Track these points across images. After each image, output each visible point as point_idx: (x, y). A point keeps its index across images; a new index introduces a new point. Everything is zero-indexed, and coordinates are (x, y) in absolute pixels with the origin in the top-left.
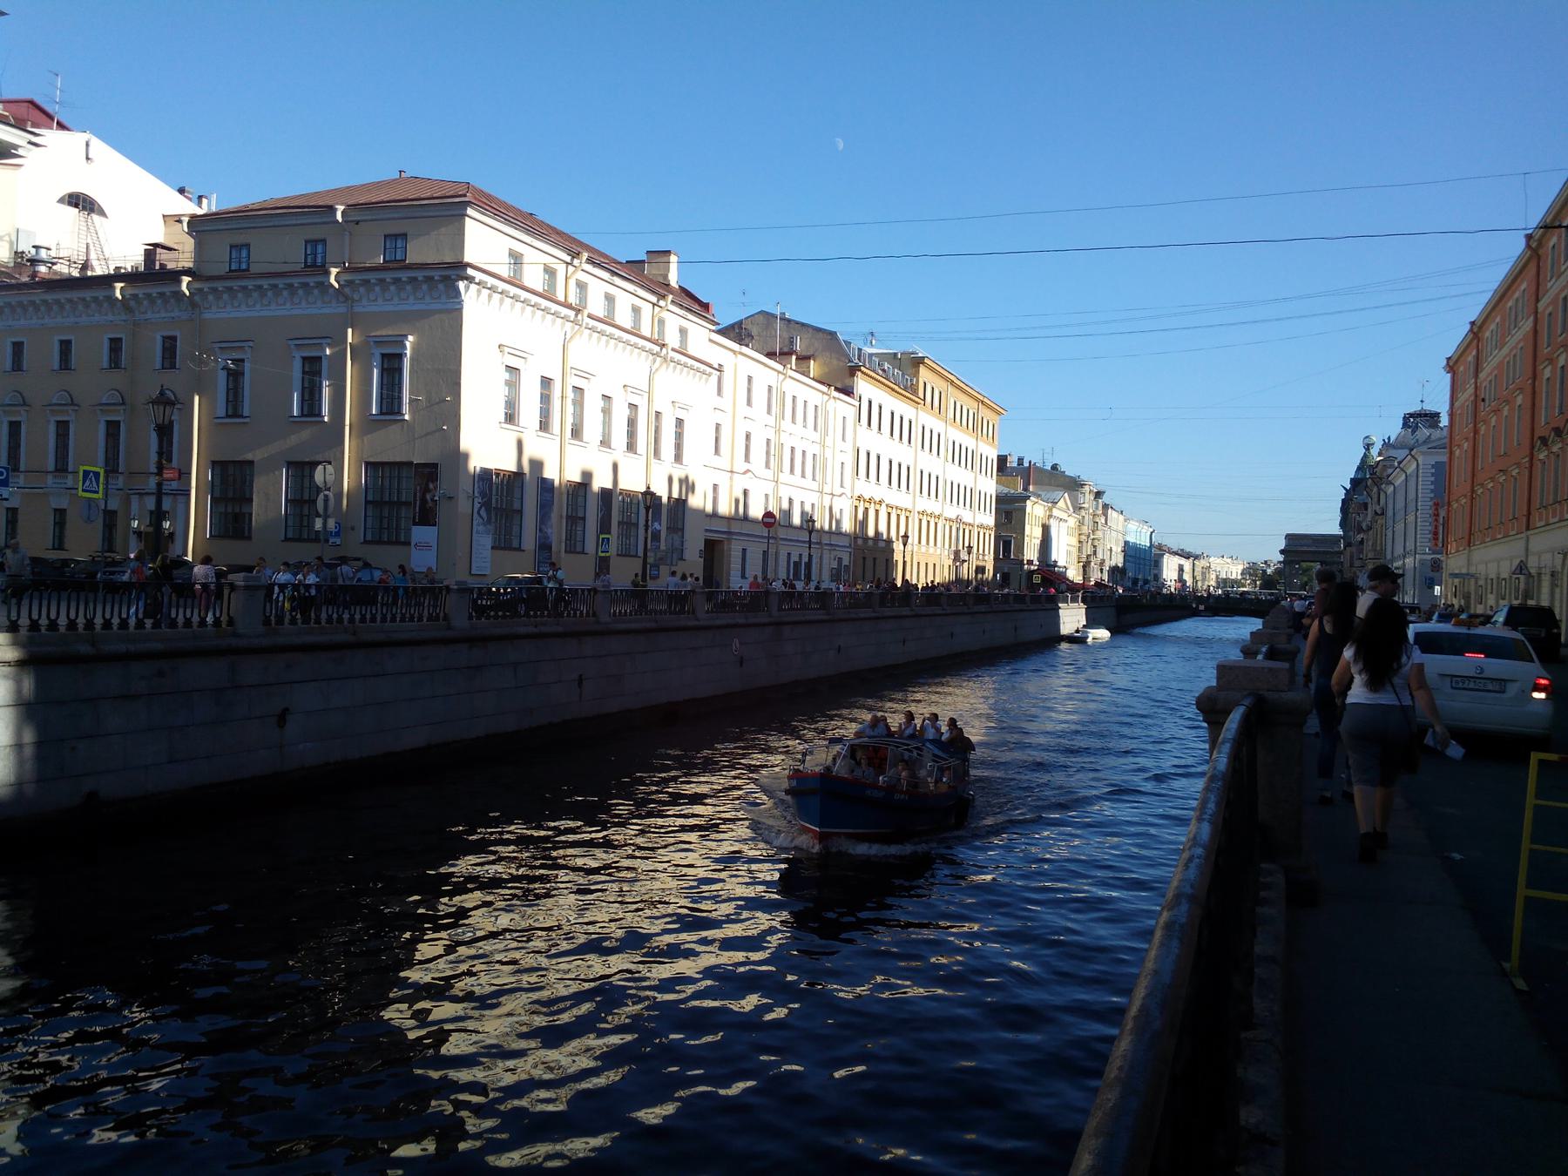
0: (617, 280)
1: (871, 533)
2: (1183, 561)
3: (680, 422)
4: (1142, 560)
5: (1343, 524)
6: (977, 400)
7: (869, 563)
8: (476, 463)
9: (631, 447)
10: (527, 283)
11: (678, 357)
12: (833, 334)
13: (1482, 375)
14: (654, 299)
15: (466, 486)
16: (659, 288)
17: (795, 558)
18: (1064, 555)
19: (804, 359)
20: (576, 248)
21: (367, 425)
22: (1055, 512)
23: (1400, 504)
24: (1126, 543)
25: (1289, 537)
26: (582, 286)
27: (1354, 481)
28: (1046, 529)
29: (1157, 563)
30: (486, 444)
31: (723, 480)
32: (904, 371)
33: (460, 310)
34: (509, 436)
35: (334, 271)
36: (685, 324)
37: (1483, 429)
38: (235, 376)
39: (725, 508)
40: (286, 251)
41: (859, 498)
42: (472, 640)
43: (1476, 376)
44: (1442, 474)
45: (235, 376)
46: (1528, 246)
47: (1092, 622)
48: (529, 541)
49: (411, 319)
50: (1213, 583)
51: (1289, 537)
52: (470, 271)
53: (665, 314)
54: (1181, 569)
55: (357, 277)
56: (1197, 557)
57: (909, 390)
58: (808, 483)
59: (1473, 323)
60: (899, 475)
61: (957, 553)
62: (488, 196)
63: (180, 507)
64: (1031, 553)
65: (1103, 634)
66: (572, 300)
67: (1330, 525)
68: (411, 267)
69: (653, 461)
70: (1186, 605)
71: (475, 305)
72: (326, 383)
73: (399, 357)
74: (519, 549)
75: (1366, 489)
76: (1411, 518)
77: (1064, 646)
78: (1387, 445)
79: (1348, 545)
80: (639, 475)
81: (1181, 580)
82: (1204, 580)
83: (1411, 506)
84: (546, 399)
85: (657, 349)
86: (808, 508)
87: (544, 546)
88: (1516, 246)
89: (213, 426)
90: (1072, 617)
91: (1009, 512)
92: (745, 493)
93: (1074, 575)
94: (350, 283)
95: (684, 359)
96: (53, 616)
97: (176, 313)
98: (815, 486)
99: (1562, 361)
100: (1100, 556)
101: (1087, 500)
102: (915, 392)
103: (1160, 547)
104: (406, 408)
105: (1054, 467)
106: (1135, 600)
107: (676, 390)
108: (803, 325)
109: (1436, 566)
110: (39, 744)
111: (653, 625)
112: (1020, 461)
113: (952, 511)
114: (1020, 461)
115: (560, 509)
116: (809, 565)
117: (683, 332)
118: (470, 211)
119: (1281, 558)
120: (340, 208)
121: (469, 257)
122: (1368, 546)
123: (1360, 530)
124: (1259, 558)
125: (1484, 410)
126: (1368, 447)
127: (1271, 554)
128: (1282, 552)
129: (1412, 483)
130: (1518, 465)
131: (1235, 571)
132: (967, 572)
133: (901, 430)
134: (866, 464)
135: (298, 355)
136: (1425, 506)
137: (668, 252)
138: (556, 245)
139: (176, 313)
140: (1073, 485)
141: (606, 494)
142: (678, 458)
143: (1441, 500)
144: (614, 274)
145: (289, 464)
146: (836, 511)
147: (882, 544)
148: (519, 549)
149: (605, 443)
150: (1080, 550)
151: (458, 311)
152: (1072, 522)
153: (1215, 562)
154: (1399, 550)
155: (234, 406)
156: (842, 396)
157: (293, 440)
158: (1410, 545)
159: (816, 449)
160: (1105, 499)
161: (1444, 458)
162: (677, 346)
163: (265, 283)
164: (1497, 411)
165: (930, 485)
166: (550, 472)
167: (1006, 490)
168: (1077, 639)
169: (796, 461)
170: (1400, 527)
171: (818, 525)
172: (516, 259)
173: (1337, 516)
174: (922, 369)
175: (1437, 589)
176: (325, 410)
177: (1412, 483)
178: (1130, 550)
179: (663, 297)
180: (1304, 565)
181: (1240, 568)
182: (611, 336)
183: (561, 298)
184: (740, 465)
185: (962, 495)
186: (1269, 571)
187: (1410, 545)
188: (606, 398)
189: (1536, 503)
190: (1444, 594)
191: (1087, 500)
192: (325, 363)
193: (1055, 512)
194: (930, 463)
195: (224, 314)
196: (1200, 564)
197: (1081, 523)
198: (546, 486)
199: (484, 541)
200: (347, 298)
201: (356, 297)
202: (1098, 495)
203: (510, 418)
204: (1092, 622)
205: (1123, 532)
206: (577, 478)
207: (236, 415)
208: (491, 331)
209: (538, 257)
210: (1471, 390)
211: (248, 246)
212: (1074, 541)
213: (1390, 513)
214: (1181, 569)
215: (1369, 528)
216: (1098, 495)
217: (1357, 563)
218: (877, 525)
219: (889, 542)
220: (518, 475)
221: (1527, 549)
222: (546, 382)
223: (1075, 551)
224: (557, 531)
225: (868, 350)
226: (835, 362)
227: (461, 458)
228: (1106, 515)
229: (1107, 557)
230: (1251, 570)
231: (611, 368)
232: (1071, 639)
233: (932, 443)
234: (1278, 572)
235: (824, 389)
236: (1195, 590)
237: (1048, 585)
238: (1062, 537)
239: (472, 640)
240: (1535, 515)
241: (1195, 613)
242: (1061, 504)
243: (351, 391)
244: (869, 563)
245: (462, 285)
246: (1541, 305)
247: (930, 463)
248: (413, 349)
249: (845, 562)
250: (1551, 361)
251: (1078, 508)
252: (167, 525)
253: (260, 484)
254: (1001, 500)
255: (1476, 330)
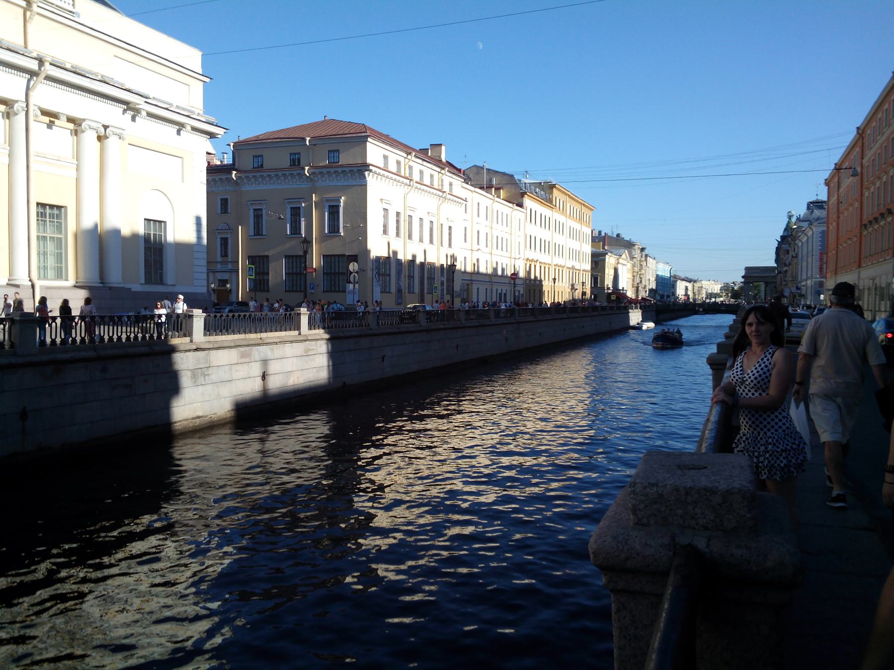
0: (425, 163)
1: (533, 277)
2: (688, 284)
3: (450, 228)
4: (666, 285)
5: (777, 261)
6: (581, 204)
7: (532, 292)
8: (374, 254)
9: (431, 242)
10: (390, 169)
11: (419, 186)
12: (512, 176)
13: (841, 190)
14: (439, 170)
15: (370, 265)
16: (438, 162)
17: (499, 291)
18: (626, 284)
19: (498, 189)
20: (410, 151)
21: (323, 238)
22: (621, 261)
23: (805, 252)
24: (657, 275)
25: (747, 269)
26: (411, 168)
27: (783, 238)
28: (616, 270)
29: (674, 286)
30: (377, 246)
31: (468, 254)
32: (546, 191)
33: (366, 185)
34: (384, 240)
35: (307, 168)
36: (423, 168)
37: (866, 194)
38: (258, 215)
39: (469, 269)
40: (278, 159)
41: (527, 259)
42: (428, 331)
43: (838, 190)
44: (824, 235)
45: (258, 215)
46: (858, 132)
47: (645, 319)
48: (393, 289)
49: (344, 189)
50: (704, 296)
51: (747, 269)
52: (371, 167)
53: (411, 163)
54: (687, 289)
55: (317, 171)
56: (695, 281)
57: (548, 201)
58: (504, 253)
59: (858, 128)
60: (545, 246)
61: (573, 285)
62: (378, 132)
63: (234, 277)
64: (609, 282)
65: (651, 325)
66: (407, 175)
67: (768, 260)
68: (342, 166)
69: (408, 241)
70: (691, 308)
71: (370, 179)
72: (302, 219)
73: (338, 207)
74: (389, 292)
75: (788, 242)
76: (810, 260)
77: (631, 331)
78: (799, 219)
79: (779, 272)
80: (437, 257)
81: (686, 295)
82: (699, 294)
83: (810, 254)
84: (398, 222)
85: (441, 194)
86: (504, 266)
87: (399, 291)
88: (850, 136)
89: (248, 239)
90: (635, 317)
91: (598, 261)
92: (478, 260)
93: (630, 294)
94: (313, 173)
95: (386, 174)
96: (53, 337)
97: (228, 188)
98: (508, 255)
99: (891, 173)
100: (643, 283)
101: (637, 253)
102: (551, 202)
103: (675, 277)
104: (341, 230)
105: (618, 235)
106: (664, 305)
107: (451, 213)
108: (497, 172)
109: (821, 284)
110: (333, 365)
111: (396, 330)
112: (600, 232)
113: (569, 264)
114: (600, 232)
115: (405, 272)
116: (505, 295)
117: (451, 184)
118: (369, 139)
119: (743, 280)
120: (308, 139)
121: (369, 161)
122: (789, 273)
123: (786, 265)
124: (730, 280)
125: (842, 207)
126: (790, 217)
127: (737, 278)
128: (743, 277)
129: (810, 240)
130: (856, 236)
131: (716, 288)
132: (578, 295)
133: (545, 223)
134: (532, 242)
135: (289, 207)
136: (816, 257)
137: (441, 145)
138: (401, 150)
139: (228, 188)
140: (629, 245)
141: (422, 264)
142: (450, 245)
143: (823, 253)
144: (424, 160)
145: (286, 257)
146: (517, 267)
147: (538, 282)
148: (389, 292)
149: (421, 240)
150: (633, 280)
151: (365, 185)
152: (629, 265)
153: (705, 283)
154: (804, 277)
155: (258, 231)
156: (519, 208)
157: (288, 245)
158: (809, 274)
159: (488, 230)
160: (646, 252)
161: (825, 229)
162: (418, 180)
163: (272, 174)
164: (847, 209)
165: (559, 250)
166: (400, 256)
167: (595, 250)
168: (638, 328)
169: (500, 244)
170: (804, 264)
171: (457, 268)
172: (386, 157)
173: (773, 256)
174: (554, 190)
175: (822, 297)
176: (303, 232)
177: (811, 238)
178: (659, 280)
179: (410, 153)
180: (756, 284)
181: (719, 286)
182: (387, 177)
183: (403, 174)
184: (475, 247)
185: (575, 254)
186: (736, 288)
187: (809, 274)
188: (421, 219)
189: (863, 256)
190: (825, 299)
191: (637, 253)
192: (302, 210)
193: (621, 261)
194: (559, 239)
195: (251, 188)
196: (697, 285)
197: (634, 266)
198: (399, 262)
199: (377, 289)
200: (312, 180)
201: (316, 179)
202: (643, 250)
203: (385, 232)
204: (645, 319)
205: (658, 268)
206: (410, 258)
207: (258, 234)
208: (380, 193)
209: (395, 156)
210: (836, 197)
211: (262, 156)
212: (630, 276)
213: (800, 256)
214: (687, 289)
215: (790, 264)
216: (643, 250)
217: (784, 283)
218: (535, 273)
219: (541, 281)
220: (389, 258)
221: (859, 277)
222: (398, 214)
223: (631, 281)
224: (404, 283)
225: (527, 181)
226: (513, 190)
227: (368, 252)
228: (646, 260)
229: (647, 284)
230: (726, 288)
231: (422, 205)
232: (634, 328)
233: (559, 228)
234: (741, 288)
235: (511, 205)
236: (694, 300)
237: (618, 303)
238: (624, 274)
239: (428, 331)
240: (862, 261)
241: (696, 313)
242: (624, 256)
243: (315, 223)
244: (532, 292)
245: (366, 173)
246: (864, 161)
247: (559, 239)
248: (344, 203)
249: (522, 292)
250: (868, 189)
251: (632, 258)
252: (228, 286)
253: (272, 266)
254: (594, 255)
255: (861, 132)
